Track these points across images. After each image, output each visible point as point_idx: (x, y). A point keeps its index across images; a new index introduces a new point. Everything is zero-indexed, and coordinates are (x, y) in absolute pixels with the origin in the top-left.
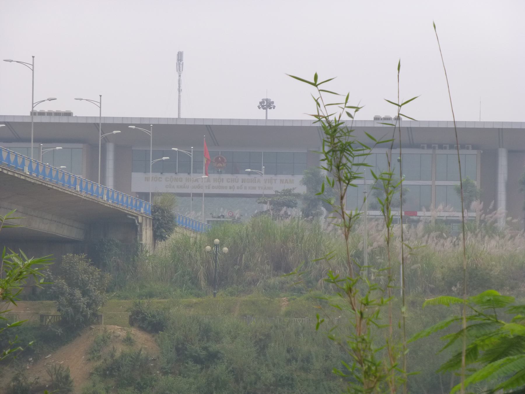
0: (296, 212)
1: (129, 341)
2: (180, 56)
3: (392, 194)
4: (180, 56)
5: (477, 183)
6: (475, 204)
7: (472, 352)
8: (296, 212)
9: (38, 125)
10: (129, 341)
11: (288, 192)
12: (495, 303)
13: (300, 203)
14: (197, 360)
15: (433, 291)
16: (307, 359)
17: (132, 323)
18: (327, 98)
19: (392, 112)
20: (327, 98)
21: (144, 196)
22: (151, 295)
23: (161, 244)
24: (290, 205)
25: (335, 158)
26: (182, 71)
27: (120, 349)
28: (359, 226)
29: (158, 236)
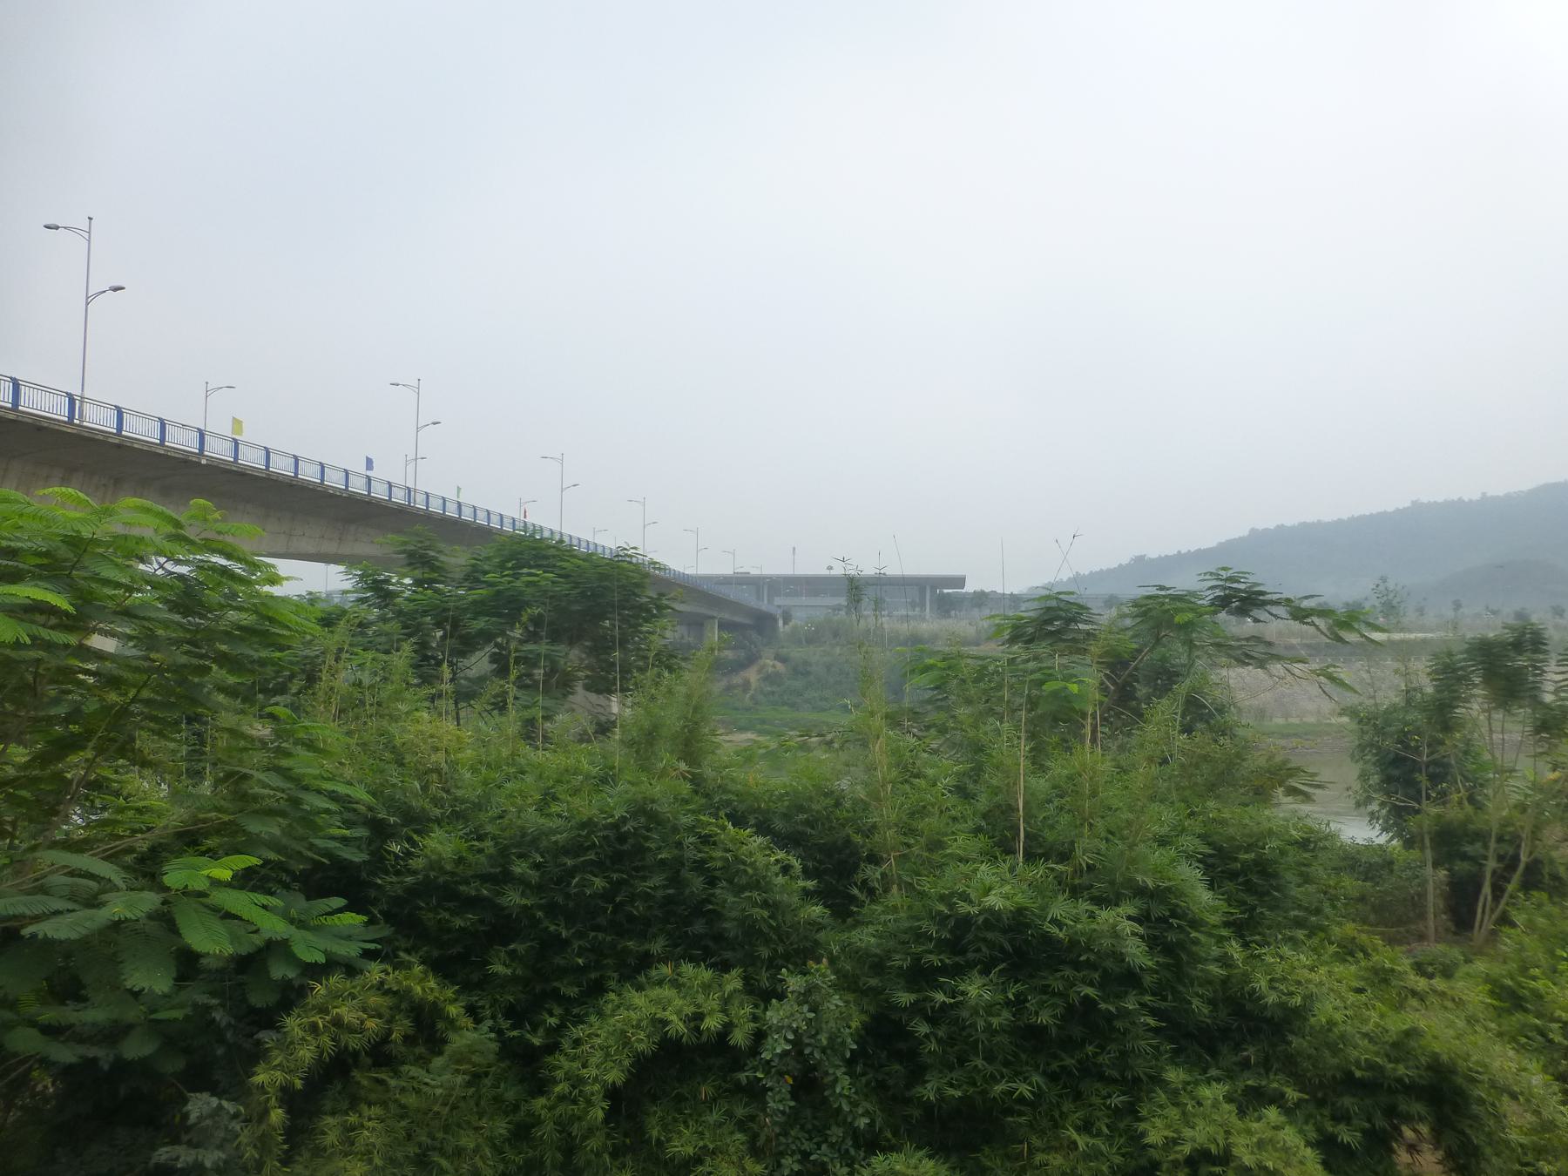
0: (843, 613)
1: (774, 666)
2: (794, 549)
3: (355, 806)
4: (794, 549)
5: (918, 600)
6: (917, 609)
7: (912, 671)
8: (843, 613)
9: (737, 578)
10: (774, 666)
11: (839, 605)
12: (922, 651)
13: (845, 609)
14: (802, 674)
15: (900, 645)
16: (848, 674)
17: (775, 659)
18: (849, 567)
19: (878, 571)
20: (849, 567)
21: (779, 606)
22: (783, 647)
23: (787, 627)
24: (839, 610)
25: (296, 669)
26: (1073, 593)
27: (770, 670)
28: (417, 822)
29: (785, 623)
